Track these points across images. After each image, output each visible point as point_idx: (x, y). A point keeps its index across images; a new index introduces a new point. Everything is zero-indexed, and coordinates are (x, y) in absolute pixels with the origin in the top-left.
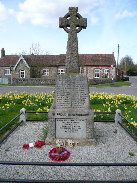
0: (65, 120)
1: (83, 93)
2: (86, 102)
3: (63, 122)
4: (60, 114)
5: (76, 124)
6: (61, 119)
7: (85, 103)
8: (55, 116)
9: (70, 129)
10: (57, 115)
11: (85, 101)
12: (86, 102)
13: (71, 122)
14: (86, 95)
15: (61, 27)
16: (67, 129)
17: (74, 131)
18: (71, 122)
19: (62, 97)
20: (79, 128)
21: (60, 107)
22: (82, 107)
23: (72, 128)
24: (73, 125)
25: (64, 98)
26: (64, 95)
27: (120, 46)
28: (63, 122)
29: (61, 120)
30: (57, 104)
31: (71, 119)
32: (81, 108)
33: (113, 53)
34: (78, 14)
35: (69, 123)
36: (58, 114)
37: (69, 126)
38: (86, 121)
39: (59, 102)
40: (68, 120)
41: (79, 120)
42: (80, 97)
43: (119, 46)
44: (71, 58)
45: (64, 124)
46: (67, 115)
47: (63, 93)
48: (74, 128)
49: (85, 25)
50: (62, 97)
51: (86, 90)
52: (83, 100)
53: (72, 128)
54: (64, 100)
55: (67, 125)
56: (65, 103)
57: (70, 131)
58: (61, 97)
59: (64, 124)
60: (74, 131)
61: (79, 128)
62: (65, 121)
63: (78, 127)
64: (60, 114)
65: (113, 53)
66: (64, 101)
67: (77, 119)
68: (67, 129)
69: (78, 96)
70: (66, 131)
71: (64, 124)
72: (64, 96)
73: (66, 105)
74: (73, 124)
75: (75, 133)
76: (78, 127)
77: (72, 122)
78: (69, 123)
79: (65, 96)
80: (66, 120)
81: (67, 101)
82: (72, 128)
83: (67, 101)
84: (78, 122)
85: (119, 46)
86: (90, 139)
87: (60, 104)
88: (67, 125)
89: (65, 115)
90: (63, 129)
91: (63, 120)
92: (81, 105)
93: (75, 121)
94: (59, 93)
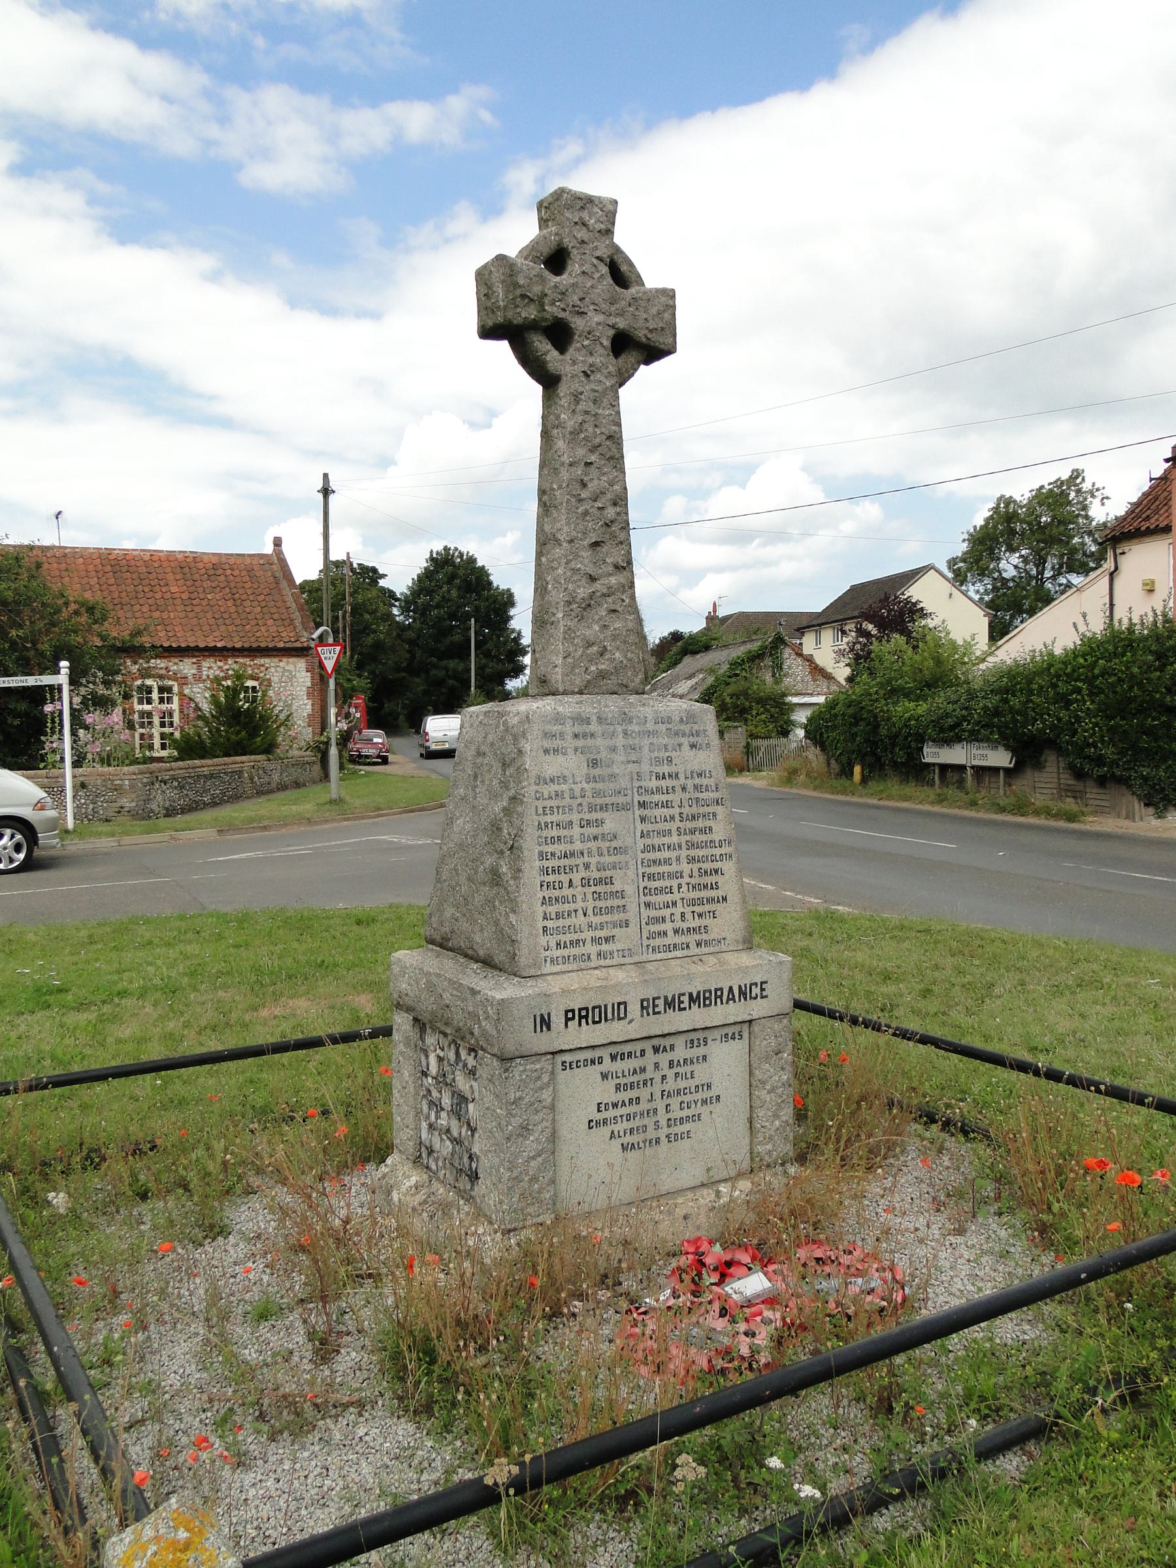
0: (613, 1058)
1: (703, 838)
2: (725, 899)
3: (604, 1076)
4: (582, 1015)
5: (688, 1068)
6: (588, 1055)
7: (719, 908)
8: (553, 1033)
9: (649, 1121)
10: (567, 1020)
11: (720, 893)
12: (725, 899)
13: (657, 1066)
14: (724, 850)
15: (488, 332)
16: (632, 1124)
17: (679, 1129)
18: (657, 1066)
19: (576, 878)
20: (704, 1102)
21: (566, 959)
22: (705, 937)
23: (661, 1110)
24: (670, 1085)
25: (585, 882)
26: (586, 859)
27: (333, 485)
28: (604, 1076)
29: (591, 1055)
30: (543, 940)
31: (656, 1042)
32: (699, 944)
33: (278, 542)
34: (618, 250)
35: (642, 1077)
36: (569, 1014)
37: (644, 1093)
38: (746, 1035)
39: (561, 923)
40: (638, 1047)
41: (701, 1035)
42: (686, 868)
43: (326, 492)
44: (592, 579)
45: (611, 1083)
46: (634, 1009)
47: (578, 846)
48: (675, 1102)
49: (659, 340)
50: (576, 878)
51: (719, 810)
52: (705, 887)
53: (661, 1110)
54: (589, 896)
55: (633, 1094)
56: (596, 920)
57: (651, 1134)
58: (565, 878)
59: (607, 1092)
60: (679, 1129)
61: (704, 1102)
62: (619, 1066)
63: (700, 1096)
64: (582, 1015)
65: (278, 542)
66: (590, 904)
67: (693, 1036)
68: (632, 1124)
69: (678, 859)
70: (628, 1139)
71: (607, 1092)
72: (587, 866)
73: (607, 940)
74: (670, 1074)
75: (685, 1144)
76: (700, 1096)
77: (663, 1059)
78: (642, 1077)
79: (593, 867)
80: (626, 1048)
81: (609, 903)
82: (660, 1105)
83: (609, 903)
84: (701, 1051)
85: (326, 492)
86: (723, 1188)
87: (568, 938)
88: (633, 1094)
89: (620, 1010)
90: (606, 1131)
91: (605, 1053)
92: (697, 923)
93: (681, 1053)
94: (550, 849)
